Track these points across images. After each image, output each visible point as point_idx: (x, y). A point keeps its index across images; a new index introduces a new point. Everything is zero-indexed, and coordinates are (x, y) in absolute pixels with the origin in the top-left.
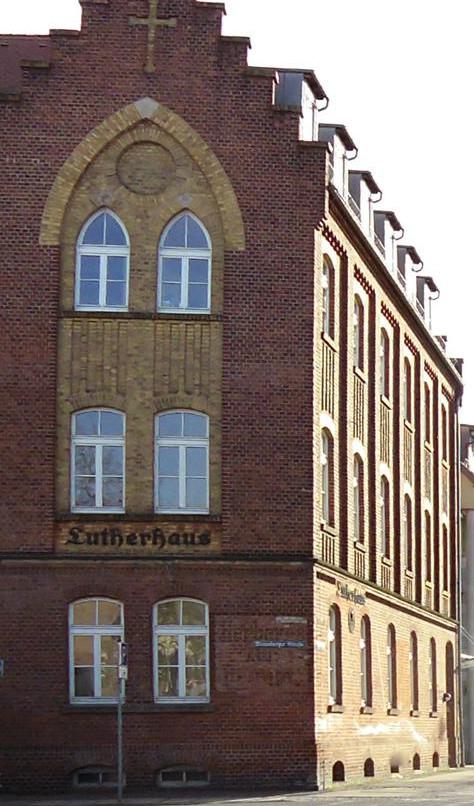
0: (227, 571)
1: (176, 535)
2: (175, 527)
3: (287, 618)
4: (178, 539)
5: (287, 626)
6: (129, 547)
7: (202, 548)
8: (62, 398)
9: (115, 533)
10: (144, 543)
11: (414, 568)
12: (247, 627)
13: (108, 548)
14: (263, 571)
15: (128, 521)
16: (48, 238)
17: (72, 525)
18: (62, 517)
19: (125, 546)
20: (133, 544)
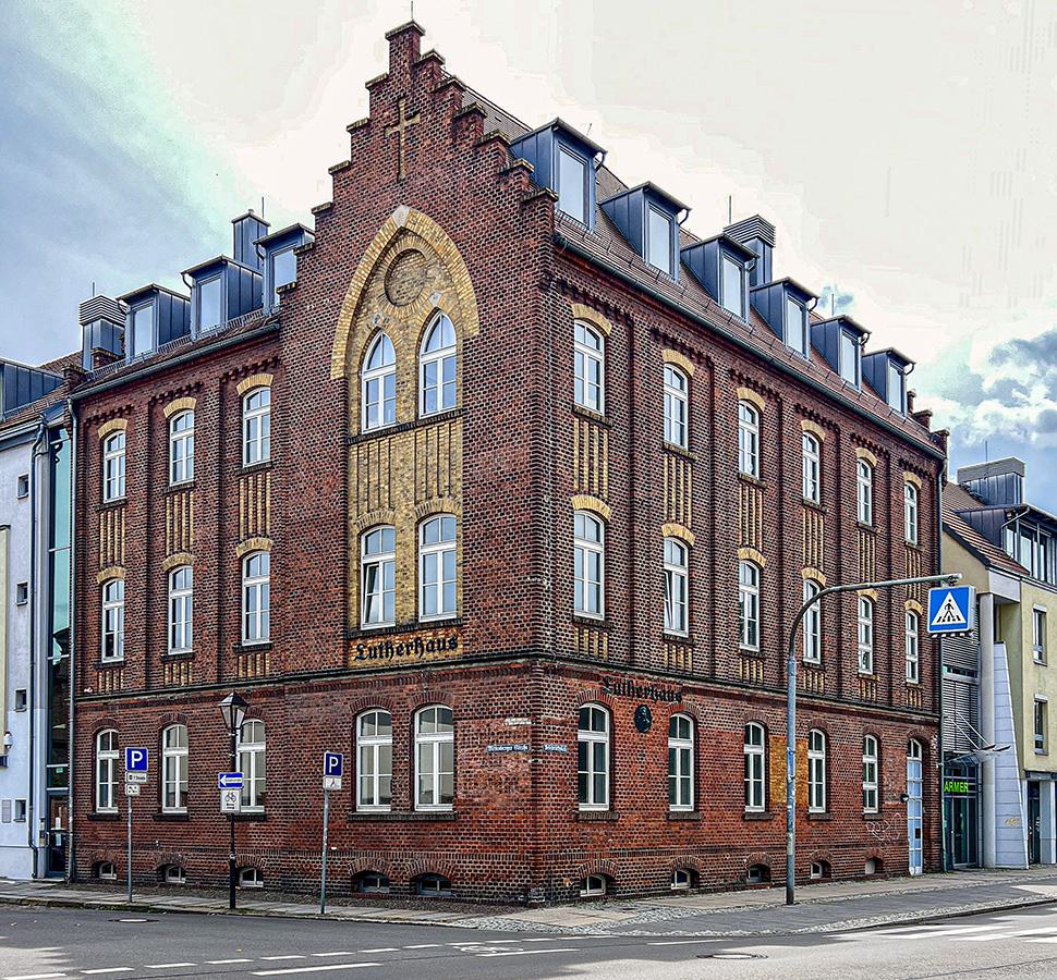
0: (466, 675)
1: (432, 642)
2: (431, 634)
3: (514, 720)
4: (433, 646)
5: (514, 728)
6: (398, 658)
7: (451, 653)
8: (352, 521)
9: (389, 645)
10: (408, 653)
11: (191, 380)
12: (482, 731)
13: (384, 661)
14: (497, 672)
15: (396, 634)
16: (337, 373)
17: (359, 642)
18: (351, 635)
19: (396, 658)
20: (401, 655)
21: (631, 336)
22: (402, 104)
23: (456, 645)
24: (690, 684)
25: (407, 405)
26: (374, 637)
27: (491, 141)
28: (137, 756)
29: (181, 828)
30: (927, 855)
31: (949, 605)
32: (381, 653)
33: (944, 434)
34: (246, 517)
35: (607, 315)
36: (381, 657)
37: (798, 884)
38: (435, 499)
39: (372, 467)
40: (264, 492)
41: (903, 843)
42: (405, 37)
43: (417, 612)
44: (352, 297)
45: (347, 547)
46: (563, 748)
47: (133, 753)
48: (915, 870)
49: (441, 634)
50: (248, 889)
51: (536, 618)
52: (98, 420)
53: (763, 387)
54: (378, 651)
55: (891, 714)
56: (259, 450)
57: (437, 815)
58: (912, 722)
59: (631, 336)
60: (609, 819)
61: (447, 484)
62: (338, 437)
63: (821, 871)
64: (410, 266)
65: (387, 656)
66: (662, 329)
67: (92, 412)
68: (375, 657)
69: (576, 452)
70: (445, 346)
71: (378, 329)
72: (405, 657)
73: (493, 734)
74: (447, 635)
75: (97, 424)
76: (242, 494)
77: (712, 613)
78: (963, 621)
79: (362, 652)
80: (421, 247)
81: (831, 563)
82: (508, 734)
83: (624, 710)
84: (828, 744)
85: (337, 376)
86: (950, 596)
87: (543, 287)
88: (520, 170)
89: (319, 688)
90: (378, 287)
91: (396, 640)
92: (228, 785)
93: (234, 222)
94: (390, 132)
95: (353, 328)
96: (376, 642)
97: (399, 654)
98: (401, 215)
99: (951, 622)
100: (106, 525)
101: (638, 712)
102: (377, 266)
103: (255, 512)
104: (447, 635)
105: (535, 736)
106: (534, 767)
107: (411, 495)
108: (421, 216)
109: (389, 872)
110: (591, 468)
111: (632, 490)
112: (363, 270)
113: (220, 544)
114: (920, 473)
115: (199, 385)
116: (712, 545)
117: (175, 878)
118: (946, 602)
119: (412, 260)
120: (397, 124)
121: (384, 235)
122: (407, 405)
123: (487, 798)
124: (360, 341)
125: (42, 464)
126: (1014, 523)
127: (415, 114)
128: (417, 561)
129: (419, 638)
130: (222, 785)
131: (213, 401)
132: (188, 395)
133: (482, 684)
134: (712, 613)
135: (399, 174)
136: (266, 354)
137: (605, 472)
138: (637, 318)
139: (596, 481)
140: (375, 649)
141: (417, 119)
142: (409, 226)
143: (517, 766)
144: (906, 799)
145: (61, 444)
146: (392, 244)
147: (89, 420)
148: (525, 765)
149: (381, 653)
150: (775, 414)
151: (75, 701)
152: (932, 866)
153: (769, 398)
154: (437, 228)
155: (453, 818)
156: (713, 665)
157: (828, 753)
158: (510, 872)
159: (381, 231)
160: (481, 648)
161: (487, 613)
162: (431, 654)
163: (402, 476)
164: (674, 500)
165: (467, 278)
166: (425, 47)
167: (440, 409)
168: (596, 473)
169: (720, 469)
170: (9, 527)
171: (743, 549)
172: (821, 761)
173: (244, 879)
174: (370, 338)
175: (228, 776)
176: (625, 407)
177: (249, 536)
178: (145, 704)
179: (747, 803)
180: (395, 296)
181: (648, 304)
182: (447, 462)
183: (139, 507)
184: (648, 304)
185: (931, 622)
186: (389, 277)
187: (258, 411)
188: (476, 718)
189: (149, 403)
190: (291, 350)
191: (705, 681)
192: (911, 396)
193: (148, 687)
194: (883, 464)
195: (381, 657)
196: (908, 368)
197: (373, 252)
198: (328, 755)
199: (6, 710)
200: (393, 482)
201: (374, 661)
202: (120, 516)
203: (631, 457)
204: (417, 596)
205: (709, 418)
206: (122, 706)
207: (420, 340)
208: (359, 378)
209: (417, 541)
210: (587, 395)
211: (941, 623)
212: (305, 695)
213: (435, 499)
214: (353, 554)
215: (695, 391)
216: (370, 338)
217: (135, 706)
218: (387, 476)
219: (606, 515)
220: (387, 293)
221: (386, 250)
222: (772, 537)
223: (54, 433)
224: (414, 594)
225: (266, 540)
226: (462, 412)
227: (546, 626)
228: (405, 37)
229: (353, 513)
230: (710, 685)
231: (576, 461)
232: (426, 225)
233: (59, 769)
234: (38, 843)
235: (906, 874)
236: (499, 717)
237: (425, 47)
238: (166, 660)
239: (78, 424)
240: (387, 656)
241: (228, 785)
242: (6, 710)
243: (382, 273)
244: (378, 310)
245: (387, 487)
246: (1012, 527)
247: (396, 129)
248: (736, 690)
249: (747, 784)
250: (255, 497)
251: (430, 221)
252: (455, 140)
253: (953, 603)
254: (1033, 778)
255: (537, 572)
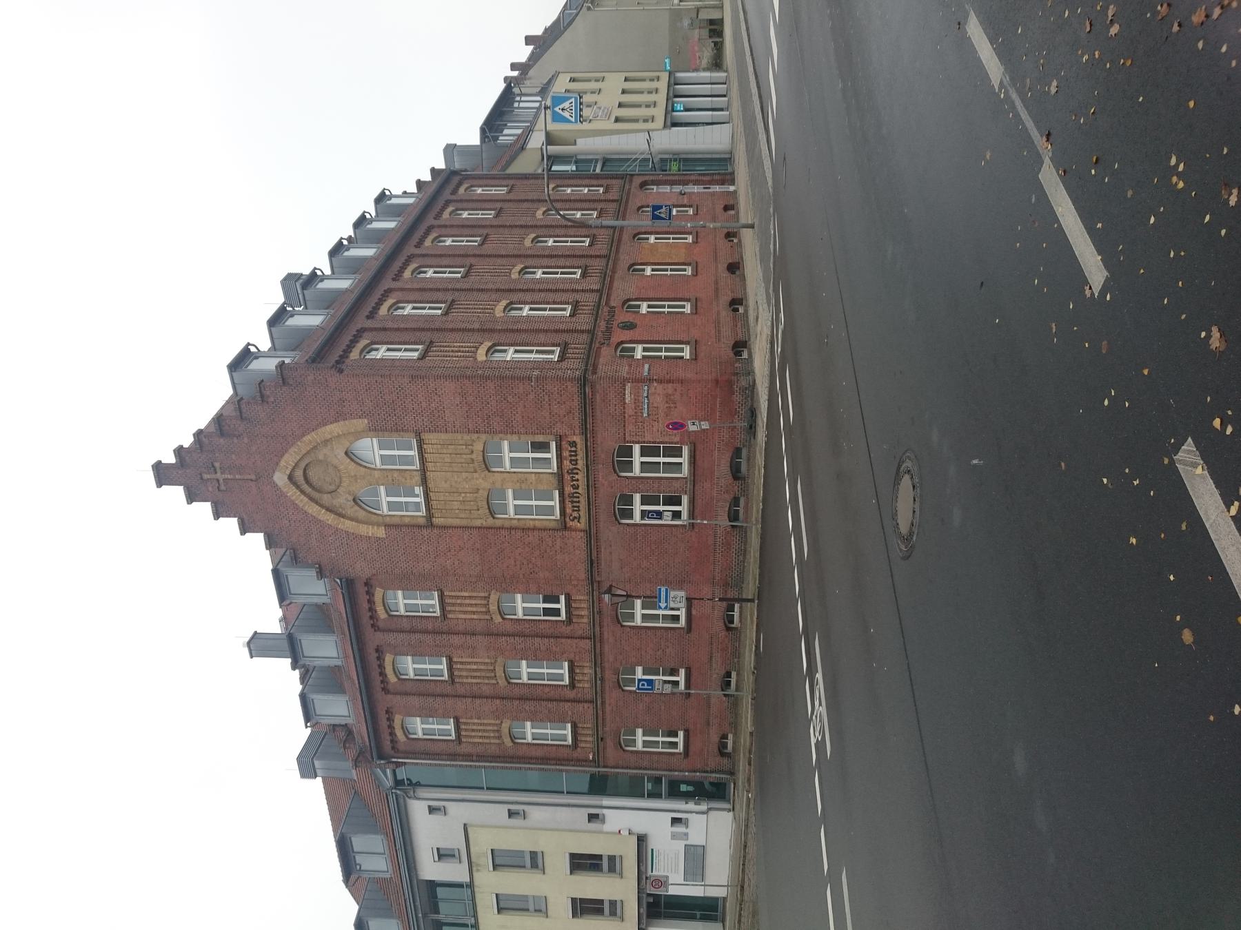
2: (565, 462)
3: (627, 396)
4: (574, 460)
5: (633, 396)
9: (572, 496)
10: (578, 480)
12: (634, 421)
16: (381, 532)
17: (567, 519)
19: (580, 490)
20: (578, 486)
21: (371, 330)
22: (206, 476)
23: (574, 442)
24: (603, 302)
25: (408, 478)
27: (240, 408)
28: (643, 685)
29: (694, 673)
30: (722, 183)
31: (563, 109)
32: (576, 502)
34: (474, 613)
35: (357, 342)
36: (579, 502)
37: (738, 221)
38: (474, 456)
39: (448, 507)
41: (713, 194)
42: (163, 474)
43: (549, 473)
44: (329, 518)
45: (502, 528)
46: (647, 366)
47: (640, 687)
48: (732, 188)
50: (741, 621)
51: (558, 379)
52: (394, 741)
53: (403, 263)
54: (575, 504)
55: (624, 200)
56: (429, 603)
58: (630, 189)
59: (371, 330)
60: (695, 346)
61: (464, 447)
62: (425, 532)
63: (736, 306)
64: (315, 474)
65: (578, 497)
66: (367, 313)
67: (387, 744)
68: (578, 507)
69: (449, 359)
70: (371, 449)
71: (354, 500)
72: (580, 483)
73: (636, 412)
74: (567, 449)
76: (459, 616)
77: (556, 291)
78: (573, 100)
79: (575, 518)
80: (303, 465)
81: (522, 231)
82: (636, 401)
83: (619, 335)
84: (637, 300)
85: (384, 532)
86: (557, 109)
87: (341, 371)
88: (261, 386)
90: (326, 499)
91: (568, 489)
92: (666, 602)
93: (252, 657)
94: (223, 487)
95: (351, 519)
96: (569, 505)
97: (577, 487)
98: (280, 478)
99: (573, 108)
100: (471, 737)
101: (623, 328)
102: (312, 499)
103: (471, 605)
105: (639, 381)
106: (660, 381)
108: (283, 463)
109: (729, 497)
110: (460, 351)
111: (473, 330)
112: (313, 509)
113: (492, 635)
114: (460, 184)
115: (378, 650)
116: (510, 290)
117: (732, 683)
118: (560, 112)
119: (310, 473)
120: (218, 480)
121: (292, 492)
122: (408, 478)
124: (361, 514)
125: (422, 792)
126: (492, 137)
127: (213, 466)
128: (515, 472)
129: (568, 472)
131: (391, 638)
132: (384, 660)
133: (602, 421)
134: (556, 291)
135: (252, 480)
136: (361, 590)
137: (461, 344)
138: (359, 326)
139: (467, 349)
140: (573, 507)
141: (217, 465)
142: (288, 472)
144: (683, 192)
145: (408, 779)
146: (298, 487)
147: (393, 748)
148: (658, 388)
149: (576, 502)
150: (421, 259)
151: (599, 767)
152: (732, 182)
153: (410, 261)
156: (592, 291)
157: (651, 233)
159: (288, 495)
160: (577, 423)
161: (553, 416)
162: (579, 462)
163: (456, 482)
164: (479, 311)
165: (328, 428)
166: (170, 459)
167: (414, 453)
168: (462, 349)
169: (458, 286)
170: (465, 825)
171: (512, 276)
172: (649, 305)
173: (733, 623)
174: (360, 507)
176: (418, 334)
177: (488, 612)
178: (603, 703)
179: (682, 358)
180: (332, 487)
182: (450, 447)
183: (460, 705)
186: (319, 491)
187: (401, 602)
190: (361, 570)
191: (601, 295)
192: (405, 193)
193: (591, 702)
194: (453, 204)
195: (579, 502)
196: (387, 193)
197: (302, 501)
199: (601, 832)
200: (460, 490)
202: (465, 724)
203: (452, 330)
204: (539, 473)
205: (425, 292)
206: (604, 725)
207: (366, 467)
208: (386, 516)
209: (501, 472)
210: (410, 354)
211: (573, 115)
213: (474, 456)
214: (507, 524)
215: (407, 299)
216: (360, 507)
217: (604, 712)
218: (456, 495)
219: (490, 344)
220: (329, 493)
221: (303, 492)
222: (504, 261)
223: (398, 783)
224: (537, 475)
225: (492, 596)
226: (418, 435)
227: (564, 373)
228: (163, 474)
229: (478, 523)
230: (604, 291)
231: (454, 359)
232: (289, 460)
233: (648, 786)
234: (704, 807)
235: (735, 192)
237: (170, 459)
238: (572, 685)
239: (395, 758)
240: (578, 497)
242: (601, 832)
243: (316, 495)
244: (342, 500)
245: (463, 495)
246: (496, 138)
247: (221, 481)
248: (608, 279)
249: (666, 357)
250: (460, 605)
251: (286, 456)
252: (234, 436)
253: (561, 107)
254: (669, 123)
255: (530, 379)
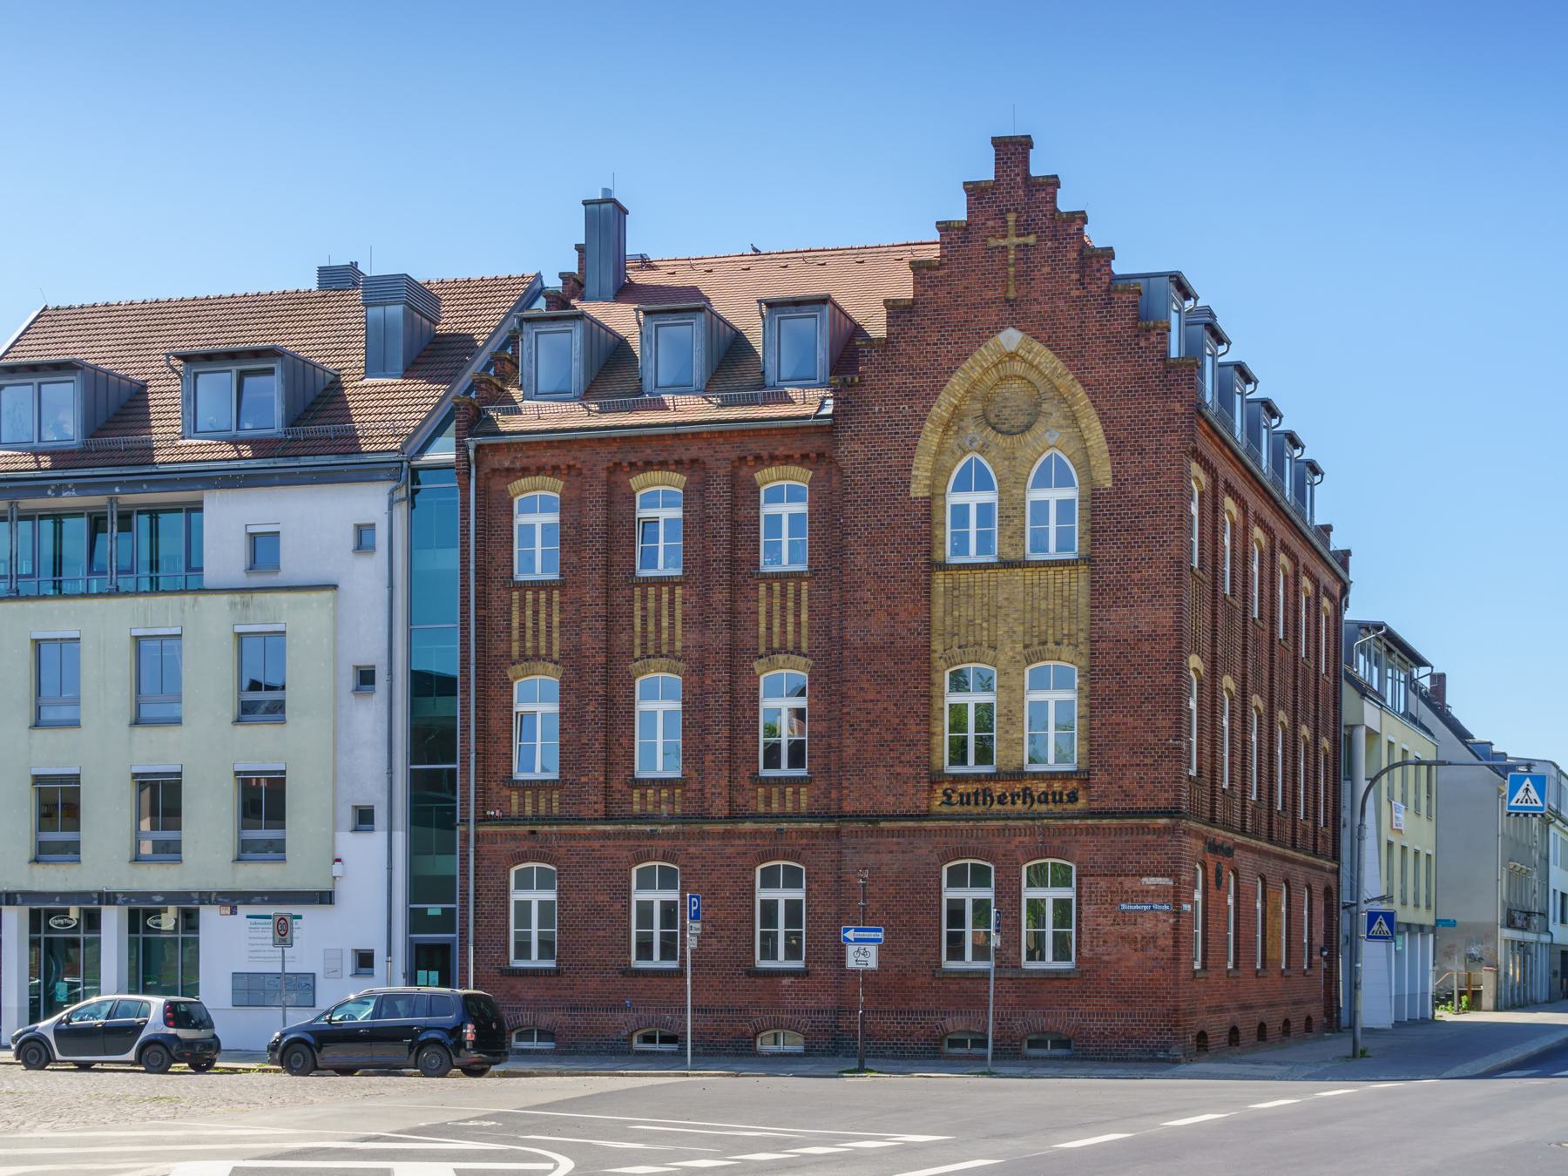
0: (1090, 831)
2: (1044, 785)
5: (1153, 888)
7: (1069, 806)
8: (937, 655)
10: (1013, 803)
19: (996, 807)
20: (1004, 804)
23: (1077, 800)
26: (966, 782)
33: (1347, 553)
40: (798, 603)
49: (1057, 786)
57: (969, 972)
65: (984, 803)
75: (507, 477)
78: (1540, 804)
79: (949, 797)
82: (1145, 893)
89: (892, 833)
92: (857, 940)
98: (1011, 338)
99: (1529, 804)
104: (1065, 788)
106: (1176, 927)
107: (1019, 636)
108: (1037, 346)
118: (1524, 786)
123: (1119, 956)
129: (1027, 788)
130: (847, 940)
143: (1156, 925)
148: (1165, 924)
154: (1058, 363)
155: (1078, 976)
158: (1148, 1030)
165: (1097, 426)
170: (335, 587)
175: (856, 930)
181: (1229, 459)
184: (1229, 459)
185: (1510, 802)
188: (1106, 875)
189: (608, 468)
195: (977, 803)
198: (691, 897)
201: (970, 808)
202: (549, 601)
211: (1519, 804)
212: (872, 840)
236: (1135, 875)
240: (984, 803)
241: (857, 940)
252: (1083, 276)
